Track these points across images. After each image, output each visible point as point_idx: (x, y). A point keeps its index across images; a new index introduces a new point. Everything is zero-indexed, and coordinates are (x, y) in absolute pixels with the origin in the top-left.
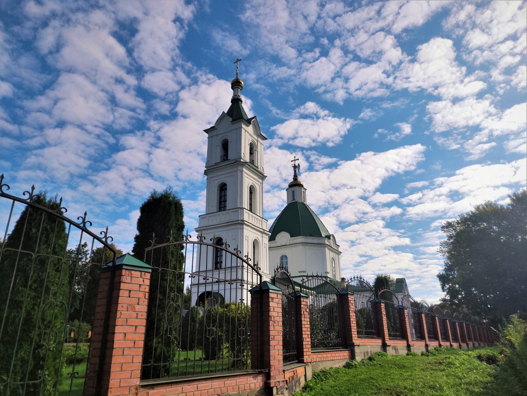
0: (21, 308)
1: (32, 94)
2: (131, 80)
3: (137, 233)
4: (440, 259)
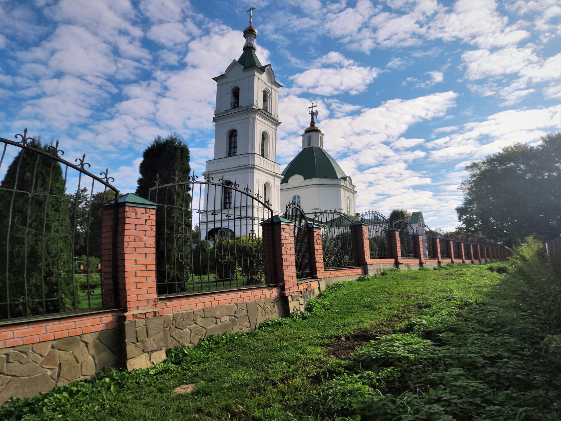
0: (24, 244)
1: (26, 45)
2: (137, 32)
3: (140, 176)
4: (460, 195)
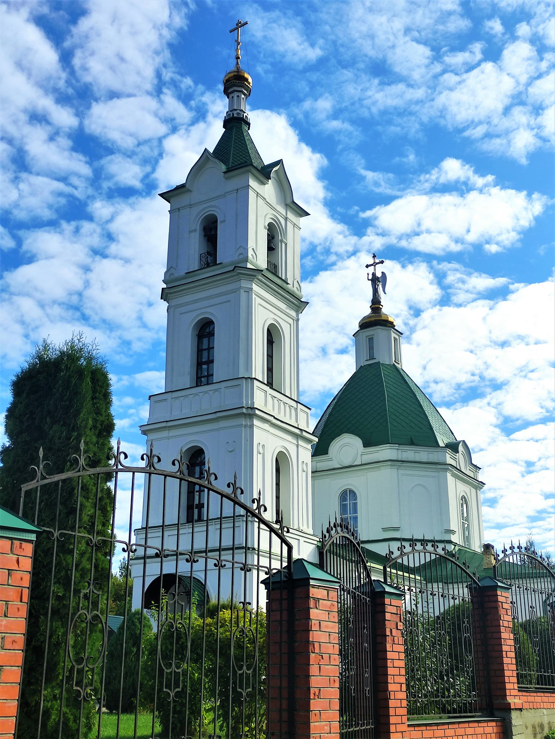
2: (64, 117)
